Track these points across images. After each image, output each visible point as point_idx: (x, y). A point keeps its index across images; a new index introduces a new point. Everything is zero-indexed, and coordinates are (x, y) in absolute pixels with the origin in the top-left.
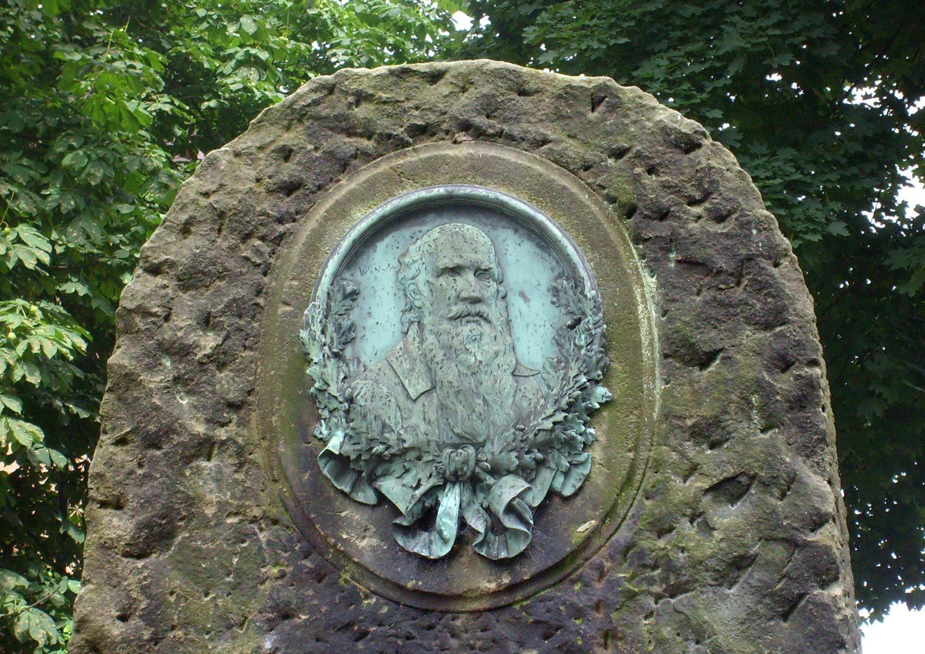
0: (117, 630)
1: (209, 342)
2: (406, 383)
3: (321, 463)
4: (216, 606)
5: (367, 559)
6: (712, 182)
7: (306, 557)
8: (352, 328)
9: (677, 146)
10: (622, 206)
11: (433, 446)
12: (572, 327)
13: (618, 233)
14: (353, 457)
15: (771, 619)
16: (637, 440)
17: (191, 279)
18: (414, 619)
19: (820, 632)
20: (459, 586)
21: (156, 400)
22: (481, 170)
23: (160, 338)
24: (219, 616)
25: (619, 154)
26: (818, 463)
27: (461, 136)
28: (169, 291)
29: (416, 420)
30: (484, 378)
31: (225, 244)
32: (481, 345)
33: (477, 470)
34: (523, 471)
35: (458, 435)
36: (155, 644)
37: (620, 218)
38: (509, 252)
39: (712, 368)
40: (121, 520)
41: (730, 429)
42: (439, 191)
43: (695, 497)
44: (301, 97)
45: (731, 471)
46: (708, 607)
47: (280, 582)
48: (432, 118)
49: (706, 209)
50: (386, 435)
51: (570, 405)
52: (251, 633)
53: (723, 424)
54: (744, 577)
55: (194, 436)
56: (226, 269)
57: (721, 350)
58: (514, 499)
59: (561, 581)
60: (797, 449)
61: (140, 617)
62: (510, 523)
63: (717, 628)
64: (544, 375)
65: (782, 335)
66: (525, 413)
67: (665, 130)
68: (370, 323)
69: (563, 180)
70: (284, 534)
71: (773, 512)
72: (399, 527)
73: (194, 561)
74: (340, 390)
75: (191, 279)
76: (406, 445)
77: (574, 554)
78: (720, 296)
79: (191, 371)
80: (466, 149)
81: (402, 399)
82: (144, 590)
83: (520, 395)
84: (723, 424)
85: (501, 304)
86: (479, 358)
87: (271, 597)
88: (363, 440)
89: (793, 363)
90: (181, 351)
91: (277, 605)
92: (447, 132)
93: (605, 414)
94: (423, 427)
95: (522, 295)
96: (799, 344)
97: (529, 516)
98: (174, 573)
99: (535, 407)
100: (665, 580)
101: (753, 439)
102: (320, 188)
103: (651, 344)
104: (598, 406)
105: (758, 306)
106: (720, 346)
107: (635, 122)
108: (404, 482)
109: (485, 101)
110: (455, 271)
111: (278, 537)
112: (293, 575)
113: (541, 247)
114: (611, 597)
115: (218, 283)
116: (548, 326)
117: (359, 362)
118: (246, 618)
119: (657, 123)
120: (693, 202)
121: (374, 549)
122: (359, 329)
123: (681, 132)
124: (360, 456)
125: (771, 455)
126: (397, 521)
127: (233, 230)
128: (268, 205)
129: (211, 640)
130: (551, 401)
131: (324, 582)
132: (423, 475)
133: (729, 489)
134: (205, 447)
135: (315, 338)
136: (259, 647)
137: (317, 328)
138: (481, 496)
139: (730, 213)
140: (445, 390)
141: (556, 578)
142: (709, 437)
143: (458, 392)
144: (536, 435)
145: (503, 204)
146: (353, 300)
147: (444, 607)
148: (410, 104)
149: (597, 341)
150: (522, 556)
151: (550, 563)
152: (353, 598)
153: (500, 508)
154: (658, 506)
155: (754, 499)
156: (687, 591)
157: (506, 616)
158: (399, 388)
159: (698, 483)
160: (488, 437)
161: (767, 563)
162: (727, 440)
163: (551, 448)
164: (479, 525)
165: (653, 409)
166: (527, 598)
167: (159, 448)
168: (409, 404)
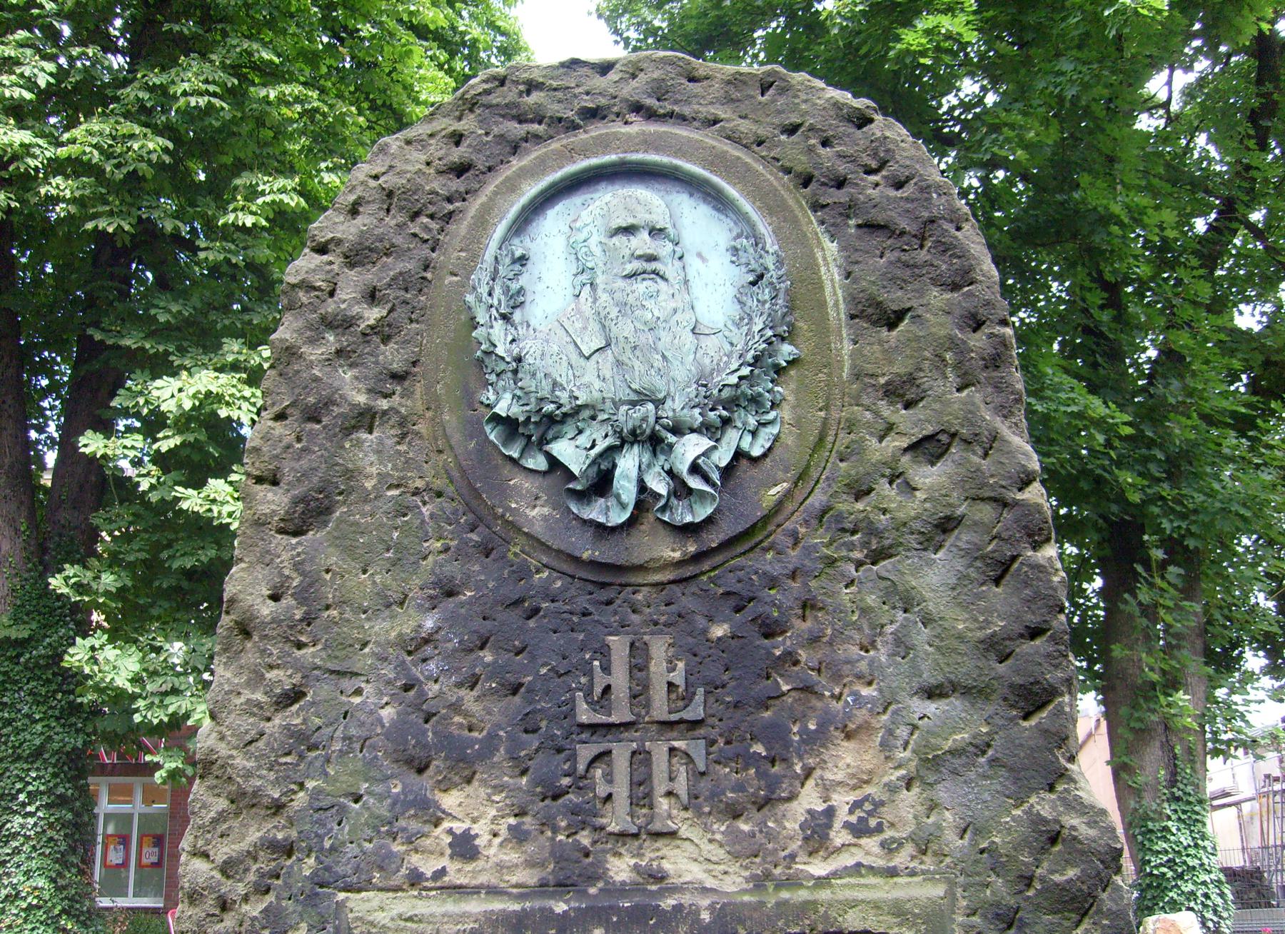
0: (267, 610)
1: (373, 315)
2: (579, 341)
3: (488, 429)
4: (374, 582)
5: (538, 529)
6: (887, 151)
7: (472, 531)
8: (521, 291)
9: (850, 121)
10: (798, 175)
11: (609, 404)
12: (753, 284)
13: (796, 201)
14: (521, 419)
15: (982, 584)
16: (828, 398)
17: (356, 257)
18: (591, 594)
19: (1037, 596)
20: (638, 558)
21: (316, 372)
22: (649, 143)
23: (323, 311)
24: (378, 594)
25: (792, 130)
26: (1016, 424)
27: (632, 117)
28: (335, 267)
29: (590, 377)
30: (663, 334)
31: (393, 223)
32: (657, 300)
33: (657, 428)
34: (706, 429)
35: (635, 391)
36: (309, 625)
37: (795, 187)
38: (685, 215)
39: (901, 327)
40: (275, 494)
41: (926, 386)
42: (612, 157)
43: (893, 456)
44: (472, 86)
45: (929, 429)
46: (915, 572)
47: (442, 556)
48: (603, 101)
49: (884, 177)
50: (557, 393)
51: (756, 358)
52: (411, 611)
53: (918, 382)
54: (951, 540)
55: (355, 406)
56: (393, 246)
57: (909, 309)
58: (698, 457)
59: (752, 549)
60: (995, 408)
61: (292, 595)
62: (695, 483)
63: (928, 595)
64: (727, 333)
65: (970, 294)
66: (708, 370)
67: (837, 106)
68: (540, 287)
69: (735, 152)
70: (448, 506)
71: (978, 470)
72: (573, 492)
73: (351, 536)
74: (507, 351)
75: (356, 257)
76: (579, 402)
77: (766, 519)
78: (905, 257)
79: (354, 343)
80: (638, 126)
81: (574, 357)
82: (297, 566)
83: (701, 352)
84: (918, 382)
85: (678, 264)
86: (657, 314)
87: (433, 572)
88: (533, 400)
89: (984, 322)
90: (343, 324)
91: (440, 580)
92: (618, 115)
93: (792, 373)
94: (597, 384)
95: (699, 255)
96: (988, 303)
97: (715, 476)
98: (331, 550)
99: (718, 364)
100: (866, 544)
101: (948, 401)
102: (490, 169)
103: (836, 304)
104: (785, 364)
105: (944, 267)
106: (908, 305)
107: (805, 101)
108: (578, 443)
109: (655, 85)
110: (629, 230)
111: (442, 509)
112: (458, 549)
113: (718, 210)
114: (807, 562)
115: (385, 259)
116: (728, 284)
117: (528, 326)
118: (406, 596)
119: (828, 100)
120: (870, 172)
121: (545, 518)
122: (528, 293)
123: (852, 107)
124: (529, 418)
125: (970, 412)
126: (571, 486)
127: (401, 209)
128: (442, 185)
129: (368, 619)
130: (736, 355)
131: (492, 556)
132: (598, 436)
133: (929, 447)
134: (366, 419)
135: (482, 296)
136: (419, 626)
137: (484, 290)
138: (662, 458)
139: (908, 179)
140: (621, 345)
141: (746, 546)
142: (902, 396)
143: (635, 347)
144: (720, 391)
145: (677, 168)
146: (522, 265)
147: (623, 580)
148: (580, 90)
149: (781, 295)
150: (709, 520)
151: (740, 529)
152: (523, 573)
153: (683, 468)
154: (854, 467)
155: (956, 457)
156: (890, 556)
157: (693, 588)
158: (572, 347)
159: (895, 443)
160: (668, 394)
161: (975, 523)
162: (922, 399)
163: (738, 405)
164: (659, 486)
165: (842, 369)
166: (714, 569)
167: (319, 422)
168: (582, 361)
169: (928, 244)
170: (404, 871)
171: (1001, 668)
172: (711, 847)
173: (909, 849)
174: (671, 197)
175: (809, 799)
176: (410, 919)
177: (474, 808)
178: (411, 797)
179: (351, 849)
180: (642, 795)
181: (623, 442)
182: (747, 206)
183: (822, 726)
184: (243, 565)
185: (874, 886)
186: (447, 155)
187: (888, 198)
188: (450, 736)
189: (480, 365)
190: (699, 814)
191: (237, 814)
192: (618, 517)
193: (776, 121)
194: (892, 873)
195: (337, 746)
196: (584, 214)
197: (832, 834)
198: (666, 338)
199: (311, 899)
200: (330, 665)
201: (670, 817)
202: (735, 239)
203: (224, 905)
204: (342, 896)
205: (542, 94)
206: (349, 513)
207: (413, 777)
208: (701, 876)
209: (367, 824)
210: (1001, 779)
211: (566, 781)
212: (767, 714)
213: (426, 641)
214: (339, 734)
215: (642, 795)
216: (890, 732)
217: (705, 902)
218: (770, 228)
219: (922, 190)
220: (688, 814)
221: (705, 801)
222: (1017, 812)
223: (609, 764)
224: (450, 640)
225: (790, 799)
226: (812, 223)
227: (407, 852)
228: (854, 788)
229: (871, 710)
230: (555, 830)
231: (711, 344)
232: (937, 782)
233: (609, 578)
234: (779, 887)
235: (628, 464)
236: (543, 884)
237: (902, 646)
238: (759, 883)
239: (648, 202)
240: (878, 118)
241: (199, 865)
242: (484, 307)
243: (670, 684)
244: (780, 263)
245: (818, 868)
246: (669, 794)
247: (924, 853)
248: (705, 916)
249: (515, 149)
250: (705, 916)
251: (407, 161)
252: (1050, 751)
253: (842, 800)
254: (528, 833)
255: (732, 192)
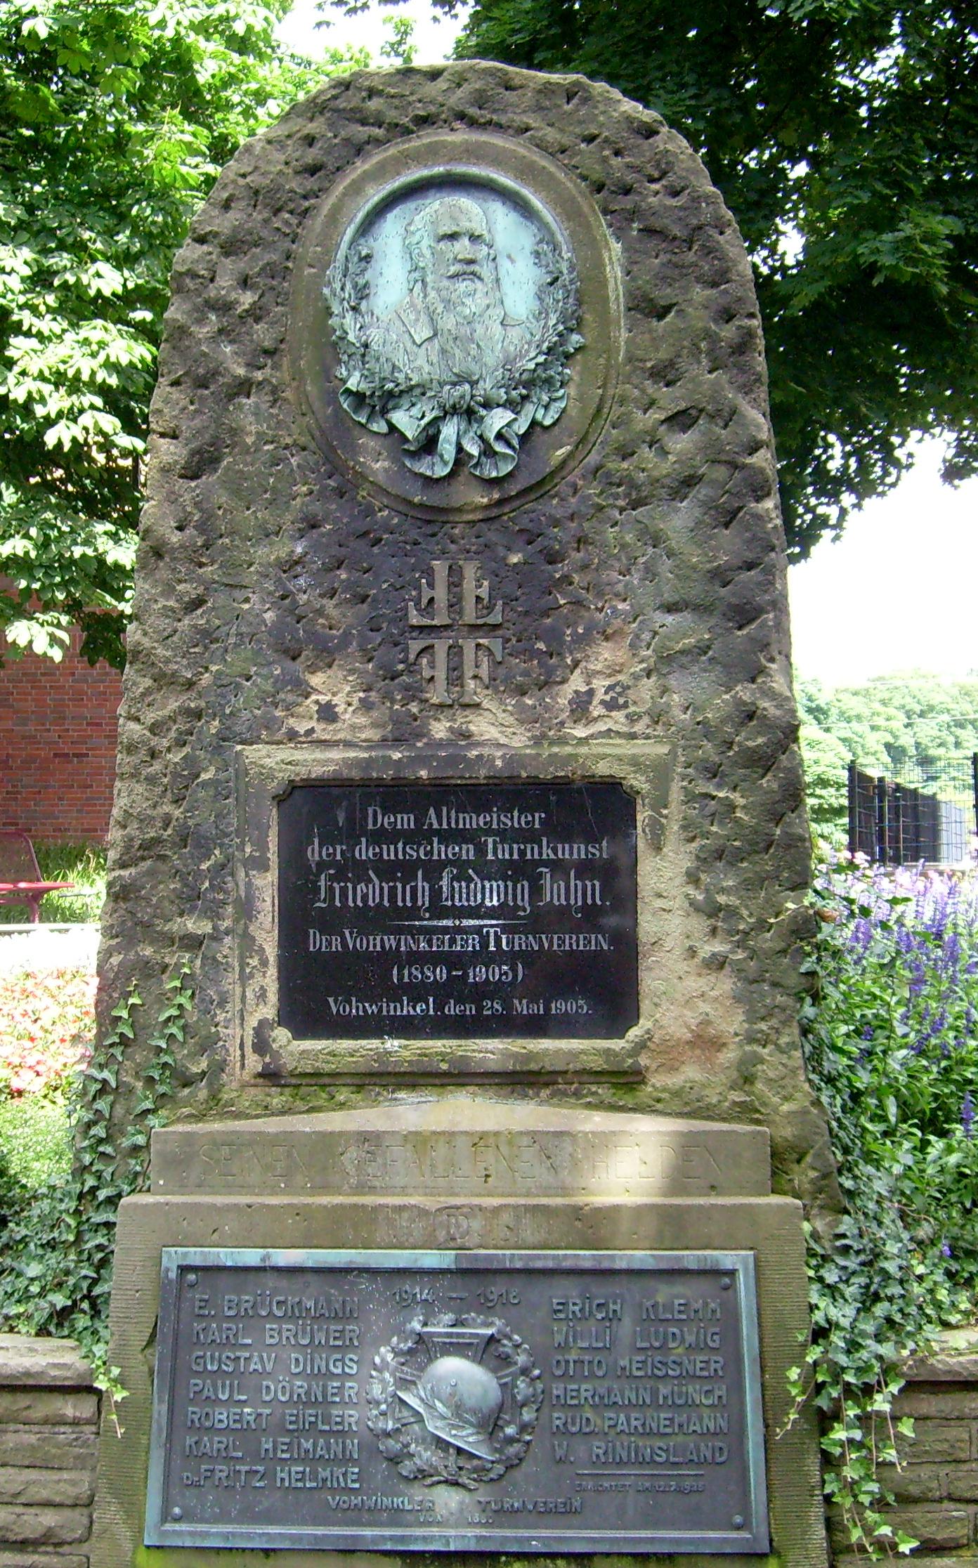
0: (175, 538)
1: (247, 299)
2: (412, 332)
3: (342, 399)
5: (381, 479)
12: (551, 284)
13: (589, 205)
14: (368, 393)
17: (231, 247)
25: (590, 139)
27: (457, 125)
28: (214, 257)
31: (260, 217)
32: (473, 299)
34: (510, 405)
37: (591, 193)
39: (667, 319)
45: (683, 406)
46: (664, 516)
51: (549, 349)
52: (285, 540)
56: (260, 238)
59: (542, 496)
62: (499, 448)
65: (726, 292)
66: (511, 358)
67: (629, 119)
70: (312, 459)
72: (408, 451)
75: (231, 247)
76: (412, 383)
77: (552, 474)
78: (674, 259)
80: (461, 136)
82: (197, 505)
87: (301, 511)
90: (224, 307)
92: (445, 122)
93: (578, 357)
94: (427, 368)
95: (509, 257)
97: (515, 442)
100: (628, 495)
101: (703, 380)
102: (338, 169)
103: (617, 298)
106: (674, 301)
107: (603, 113)
110: (453, 237)
112: (320, 492)
120: (652, 180)
121: (386, 470)
128: (296, 184)
129: (252, 546)
130: (534, 345)
133: (681, 420)
134: (244, 387)
135: (336, 291)
137: (337, 286)
138: (476, 425)
139: (683, 189)
145: (492, 180)
147: (445, 519)
148: (414, 98)
149: (572, 294)
150: (510, 474)
152: (369, 511)
153: (491, 436)
158: (407, 336)
159: (656, 415)
161: (712, 481)
164: (473, 449)
167: (207, 388)
169: (695, 247)
170: (284, 730)
171: (723, 592)
172: (504, 715)
173: (646, 720)
174: (485, 205)
175: (576, 683)
176: (290, 763)
177: (334, 686)
178: (288, 678)
179: (245, 715)
180: (455, 677)
181: (446, 413)
182: (548, 216)
183: (588, 630)
184: (153, 503)
185: (619, 745)
186: (302, 157)
187: (666, 207)
188: (315, 633)
189: (332, 348)
190: (497, 691)
191: (159, 690)
192: (441, 471)
193: (577, 130)
194: (633, 736)
195: (232, 640)
196: (417, 218)
197: (591, 708)
198: (480, 330)
199: (218, 750)
200: (225, 580)
201: (475, 693)
202: (538, 243)
203: (153, 754)
204: (239, 747)
205: (382, 100)
206: (235, 463)
207: (289, 663)
208: (498, 735)
209: (256, 696)
210: (716, 673)
211: (401, 667)
212: (549, 621)
213: (296, 563)
214: (233, 631)
215: (455, 677)
216: (637, 636)
217: (500, 754)
218: (566, 233)
219: (693, 200)
220: (489, 692)
221: (504, 684)
222: (727, 697)
223: (432, 655)
224: (315, 562)
225: (562, 682)
226: (602, 227)
227: (286, 717)
228: (610, 676)
229: (624, 620)
230: (393, 701)
231: (514, 334)
232: (669, 673)
233: (433, 517)
234: (551, 744)
235: (449, 431)
236: (384, 740)
237: (650, 573)
238: (538, 741)
239: (471, 210)
240: (665, 129)
241: (132, 726)
242: (338, 300)
243: (477, 597)
244: (572, 268)
245: (580, 732)
246: (475, 677)
247: (657, 723)
248: (499, 763)
249: (359, 150)
250: (499, 763)
251: (269, 162)
252: (755, 653)
253: (600, 684)
254: (373, 703)
255: (536, 202)
